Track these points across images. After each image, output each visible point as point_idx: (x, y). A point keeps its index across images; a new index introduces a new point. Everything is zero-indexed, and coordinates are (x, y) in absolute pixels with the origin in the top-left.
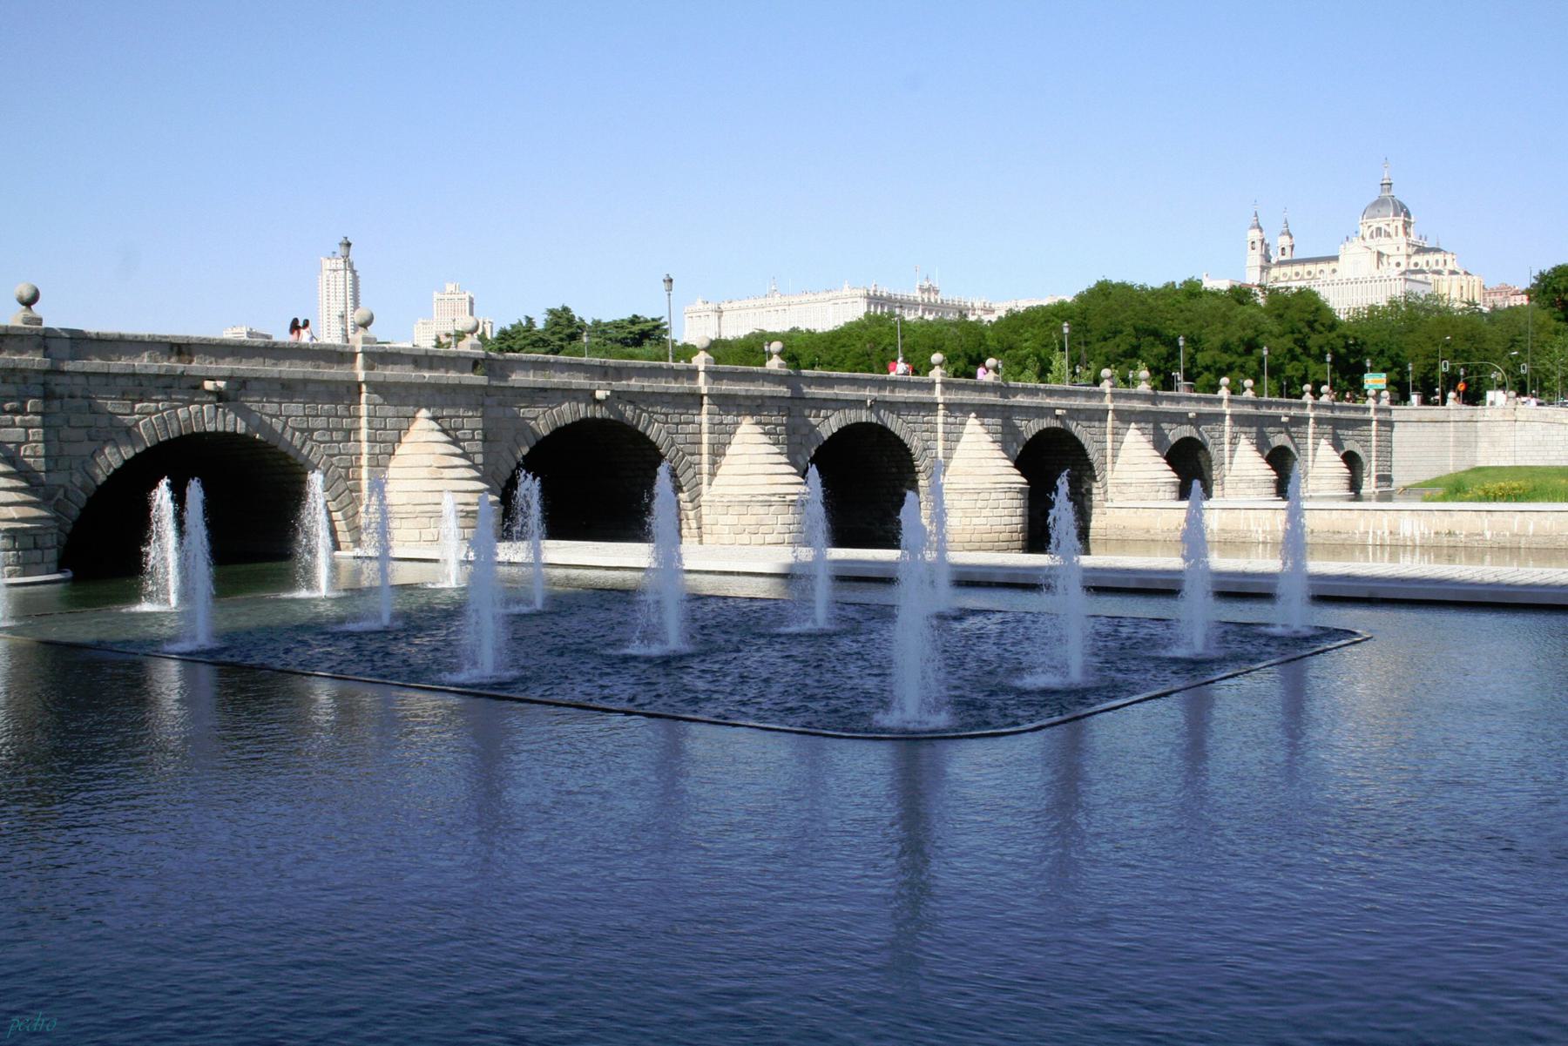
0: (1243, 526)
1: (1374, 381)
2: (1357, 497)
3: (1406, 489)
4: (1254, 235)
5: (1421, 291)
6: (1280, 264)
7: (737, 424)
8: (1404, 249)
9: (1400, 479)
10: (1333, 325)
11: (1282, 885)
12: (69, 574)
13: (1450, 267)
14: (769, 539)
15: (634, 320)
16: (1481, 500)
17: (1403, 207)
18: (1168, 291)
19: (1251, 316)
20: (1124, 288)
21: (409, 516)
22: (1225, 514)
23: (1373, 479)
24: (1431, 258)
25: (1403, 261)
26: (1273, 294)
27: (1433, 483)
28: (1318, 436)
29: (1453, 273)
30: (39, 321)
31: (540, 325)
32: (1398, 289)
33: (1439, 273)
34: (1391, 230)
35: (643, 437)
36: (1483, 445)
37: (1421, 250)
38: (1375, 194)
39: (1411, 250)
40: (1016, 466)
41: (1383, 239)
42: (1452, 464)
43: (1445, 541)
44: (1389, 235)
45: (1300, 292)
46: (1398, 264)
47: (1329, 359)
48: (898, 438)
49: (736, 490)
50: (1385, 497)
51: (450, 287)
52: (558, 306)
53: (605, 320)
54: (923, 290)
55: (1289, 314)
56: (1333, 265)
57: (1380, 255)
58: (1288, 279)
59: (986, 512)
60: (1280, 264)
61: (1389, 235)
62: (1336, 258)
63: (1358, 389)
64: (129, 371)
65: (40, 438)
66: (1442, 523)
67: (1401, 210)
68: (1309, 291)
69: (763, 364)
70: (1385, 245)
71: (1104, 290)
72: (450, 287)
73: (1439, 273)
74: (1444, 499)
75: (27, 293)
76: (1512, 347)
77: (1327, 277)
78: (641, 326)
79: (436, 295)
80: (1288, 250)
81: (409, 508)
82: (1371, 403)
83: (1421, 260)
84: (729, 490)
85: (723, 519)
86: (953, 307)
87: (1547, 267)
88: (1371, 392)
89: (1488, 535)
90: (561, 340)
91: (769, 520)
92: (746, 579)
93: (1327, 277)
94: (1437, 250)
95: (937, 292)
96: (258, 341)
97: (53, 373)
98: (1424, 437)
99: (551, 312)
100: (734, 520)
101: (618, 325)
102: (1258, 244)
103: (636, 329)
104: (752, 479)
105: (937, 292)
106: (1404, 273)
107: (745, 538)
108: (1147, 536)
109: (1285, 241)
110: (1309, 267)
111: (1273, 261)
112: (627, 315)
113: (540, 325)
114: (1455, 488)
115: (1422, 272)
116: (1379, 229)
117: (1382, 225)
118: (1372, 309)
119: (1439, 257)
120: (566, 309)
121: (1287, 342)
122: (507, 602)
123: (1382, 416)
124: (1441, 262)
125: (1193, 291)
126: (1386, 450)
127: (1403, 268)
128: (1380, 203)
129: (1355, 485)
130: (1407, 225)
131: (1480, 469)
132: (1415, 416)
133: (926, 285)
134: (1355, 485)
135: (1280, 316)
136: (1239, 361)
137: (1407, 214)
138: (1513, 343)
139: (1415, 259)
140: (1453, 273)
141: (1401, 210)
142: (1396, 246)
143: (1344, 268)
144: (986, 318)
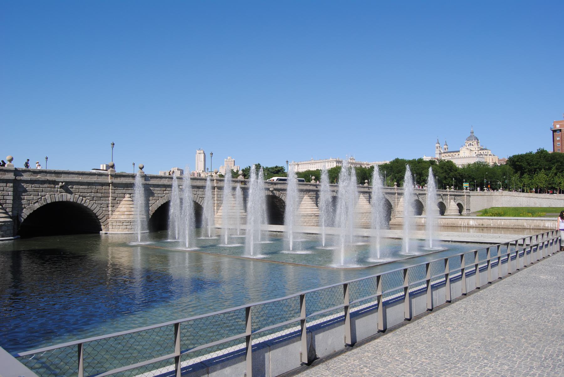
1: (466, 185)
2: (461, 215)
3: (474, 213)
4: (438, 145)
5: (482, 160)
6: (444, 153)
7: (304, 196)
9: (472, 210)
10: (456, 169)
14: (311, 224)
15: (276, 167)
16: (491, 216)
21: (236, 220)
24: (485, 151)
26: (441, 161)
28: (450, 199)
29: (490, 155)
30: (144, 173)
32: (476, 160)
33: (486, 155)
34: (474, 144)
37: (482, 149)
38: (469, 134)
42: (486, 206)
50: (468, 215)
51: (229, 158)
52: (257, 164)
53: (269, 167)
55: (445, 167)
58: (446, 158)
60: (444, 153)
62: (459, 151)
63: (461, 188)
66: (481, 222)
70: (472, 148)
72: (229, 158)
73: (486, 155)
74: (482, 216)
75: (141, 167)
77: (457, 156)
79: (225, 160)
82: (465, 191)
83: (482, 152)
86: (359, 164)
87: (511, 156)
91: (311, 219)
92: (476, 245)
93: (457, 156)
94: (486, 149)
98: (479, 199)
100: (303, 220)
101: (272, 168)
103: (276, 169)
107: (305, 224)
110: (452, 154)
112: (275, 166)
114: (485, 213)
118: (469, 165)
120: (259, 164)
121: (444, 174)
123: (468, 194)
126: (468, 203)
128: (471, 136)
129: (460, 211)
130: (478, 143)
132: (479, 194)
134: (460, 211)
135: (442, 168)
137: (478, 140)
138: (504, 174)
140: (490, 155)
142: (475, 148)
143: (462, 154)
144: (367, 167)
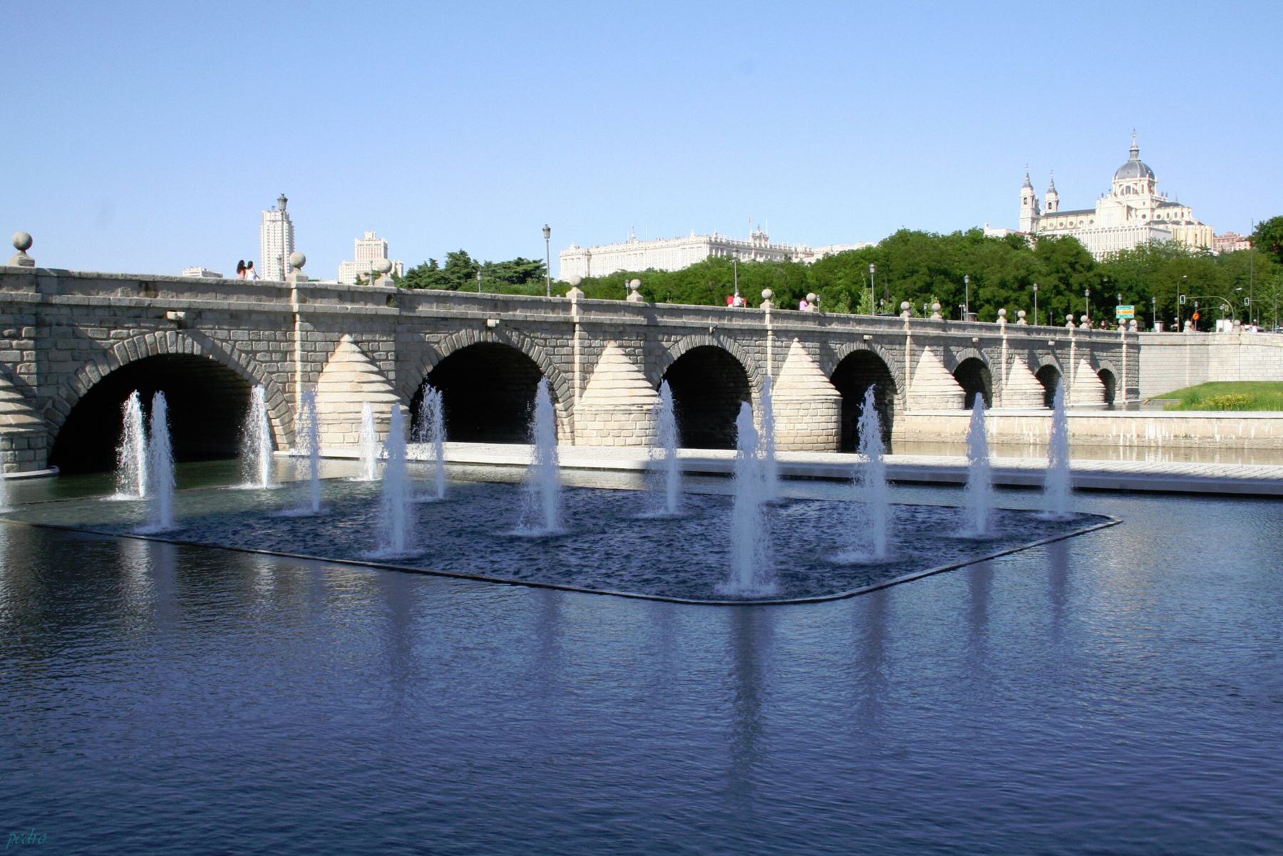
0: (1017, 431)
1: (1124, 312)
2: (1111, 407)
3: (1150, 400)
4: (1026, 192)
5: (1163, 238)
6: (1048, 216)
7: (603, 347)
8: (1148, 204)
9: (1146, 392)
10: (1091, 266)
11: (1049, 724)
12: (57, 470)
13: (1186, 218)
14: (629, 441)
15: (519, 262)
16: (1211, 409)
17: (1148, 169)
18: (956, 238)
19: (1024, 259)
20: (920, 235)
21: (335, 423)
22: (1002, 420)
23: (1124, 392)
24: (1171, 211)
25: (1148, 213)
26: (1042, 240)
27: (1173, 396)
28: (1078, 357)
29: (1189, 223)
30: (32, 263)
31: (442, 266)
32: (1144, 237)
33: (1177, 223)
34: (1138, 188)
35: (526, 358)
36: (1214, 364)
37: (1163, 205)
38: (1125, 158)
39: (1154, 205)
40: (831, 382)
41: (1132, 196)
42: (1188, 379)
43: (1182, 443)
44: (1136, 192)
45: (1064, 239)
46: (1144, 216)
47: (1087, 294)
48: (734, 358)
49: (602, 401)
50: (1134, 407)
51: (368, 235)
52: (456, 251)
53: (495, 262)
54: (755, 238)
55: (1055, 257)
56: (1091, 217)
57: (1129, 208)
58: (1054, 228)
59: (807, 419)
60: (1048, 216)
61: (1136, 192)
62: (1093, 212)
63: (1111, 318)
64: (106, 303)
65: (33, 358)
66: (1180, 428)
67: (1147, 171)
68: (1071, 238)
69: (624, 298)
70: (1133, 200)
71: (903, 238)
72: (368, 235)
73: (1177, 223)
74: (1181, 408)
75: (22, 240)
76: (1237, 284)
77: (1086, 226)
78: (525, 267)
79: (357, 242)
80: (1054, 205)
81: (335, 416)
82: (1122, 330)
83: (1163, 212)
84: (597, 401)
85: (591, 425)
86: (780, 251)
87: (1266, 218)
88: (1122, 321)
89: (1218, 438)
90: (459, 278)
91: (630, 425)
92: (611, 473)
93: (1086, 226)
94: (1176, 205)
95: (766, 239)
96: (211, 279)
97: (43, 305)
98: (1166, 358)
99: (451, 255)
100: (601, 425)
101: (505, 266)
102: (1029, 200)
103: (520, 269)
104: (615, 392)
105: (766, 239)
106: (1149, 224)
107: (610, 440)
108: (938, 439)
109: (1051, 197)
110: (1071, 219)
111: (1042, 213)
112: (513, 258)
113: (442, 266)
114: (1191, 399)
115: (1163, 222)
116: (1128, 187)
117: (1131, 184)
118: (1123, 253)
119: (1178, 210)
120: (463, 253)
121: (1053, 280)
122: (415, 493)
123: (1131, 341)
124: (1179, 215)
125: (976, 238)
126: (1134, 368)
127: (1148, 219)
128: (1129, 166)
129: (1108, 397)
130: (1151, 184)
131: (1211, 384)
132: (1158, 340)
133: (758, 233)
134: (1108, 397)
135: (1047, 259)
136: (1014, 295)
137: (1152, 175)
138: (1238, 281)
139: (1158, 212)
140: (1189, 223)
141: (1147, 171)
142: (1142, 201)
143: (1100, 219)
144: (807, 260)
